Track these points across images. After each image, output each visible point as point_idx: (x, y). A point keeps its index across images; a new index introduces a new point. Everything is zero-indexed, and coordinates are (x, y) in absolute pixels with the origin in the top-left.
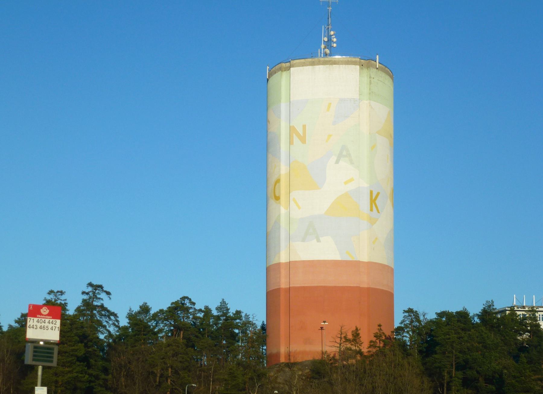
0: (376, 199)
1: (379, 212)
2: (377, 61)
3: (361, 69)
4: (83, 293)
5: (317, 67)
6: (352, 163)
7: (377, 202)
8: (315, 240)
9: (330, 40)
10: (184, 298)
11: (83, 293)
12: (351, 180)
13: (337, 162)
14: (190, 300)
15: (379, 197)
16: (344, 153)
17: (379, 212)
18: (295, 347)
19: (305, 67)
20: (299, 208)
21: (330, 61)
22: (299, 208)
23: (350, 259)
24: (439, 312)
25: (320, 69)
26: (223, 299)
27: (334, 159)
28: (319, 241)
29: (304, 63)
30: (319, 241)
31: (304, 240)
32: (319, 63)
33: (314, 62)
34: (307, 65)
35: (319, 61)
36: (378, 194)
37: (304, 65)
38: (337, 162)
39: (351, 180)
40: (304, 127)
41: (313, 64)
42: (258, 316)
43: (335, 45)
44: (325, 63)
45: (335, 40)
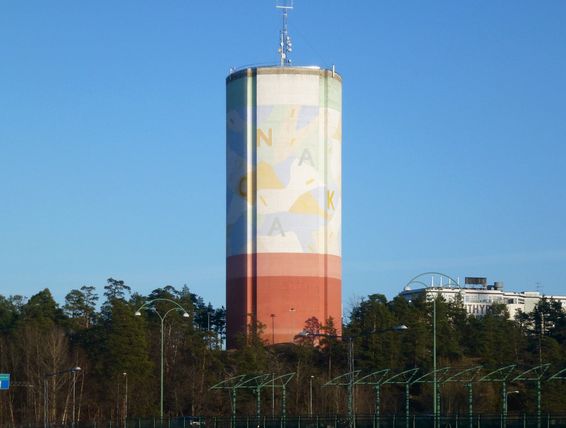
0: (331, 198)
1: (333, 209)
2: (334, 71)
3: (320, 78)
4: (106, 288)
5: (282, 76)
6: (313, 165)
7: (333, 200)
8: (280, 235)
9: (286, 45)
10: (169, 287)
11: (106, 288)
12: (312, 181)
13: (300, 164)
14: (173, 288)
15: (334, 195)
16: (306, 156)
17: (333, 209)
18: (277, 332)
19: (270, 75)
20: (266, 205)
21: (293, 71)
22: (266, 205)
23: (311, 252)
24: (371, 294)
25: (284, 77)
26: (185, 285)
27: (297, 161)
28: (283, 235)
29: (270, 71)
30: (283, 235)
31: (270, 234)
32: (284, 72)
33: (278, 71)
34: (273, 73)
35: (284, 70)
36: (333, 192)
37: (269, 73)
38: (300, 164)
39: (312, 181)
40: (270, 131)
41: (278, 72)
42: (216, 298)
43: (290, 50)
44: (289, 72)
45: (290, 45)
